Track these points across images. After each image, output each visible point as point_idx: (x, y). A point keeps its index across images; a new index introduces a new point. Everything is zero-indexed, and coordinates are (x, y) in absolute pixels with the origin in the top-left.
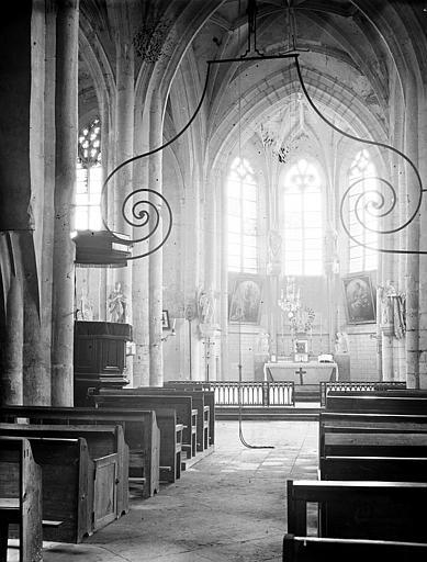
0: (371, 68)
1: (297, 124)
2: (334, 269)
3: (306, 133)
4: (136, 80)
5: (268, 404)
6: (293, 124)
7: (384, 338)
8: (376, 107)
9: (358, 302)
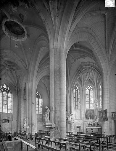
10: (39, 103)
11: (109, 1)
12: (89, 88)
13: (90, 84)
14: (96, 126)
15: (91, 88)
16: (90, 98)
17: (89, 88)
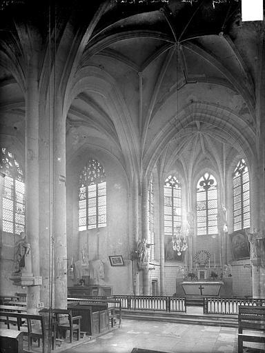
0: (241, 83)
1: (201, 151)
2: (224, 230)
3: (208, 157)
4: (38, 81)
5: (170, 311)
6: (198, 152)
7: (253, 267)
8: (247, 116)
9: (239, 247)
10: (14, 197)
11: (250, 11)
12: (170, 180)
13: (175, 171)
14: (210, 280)
15: (176, 183)
16: (173, 207)
17: (240, 166)
